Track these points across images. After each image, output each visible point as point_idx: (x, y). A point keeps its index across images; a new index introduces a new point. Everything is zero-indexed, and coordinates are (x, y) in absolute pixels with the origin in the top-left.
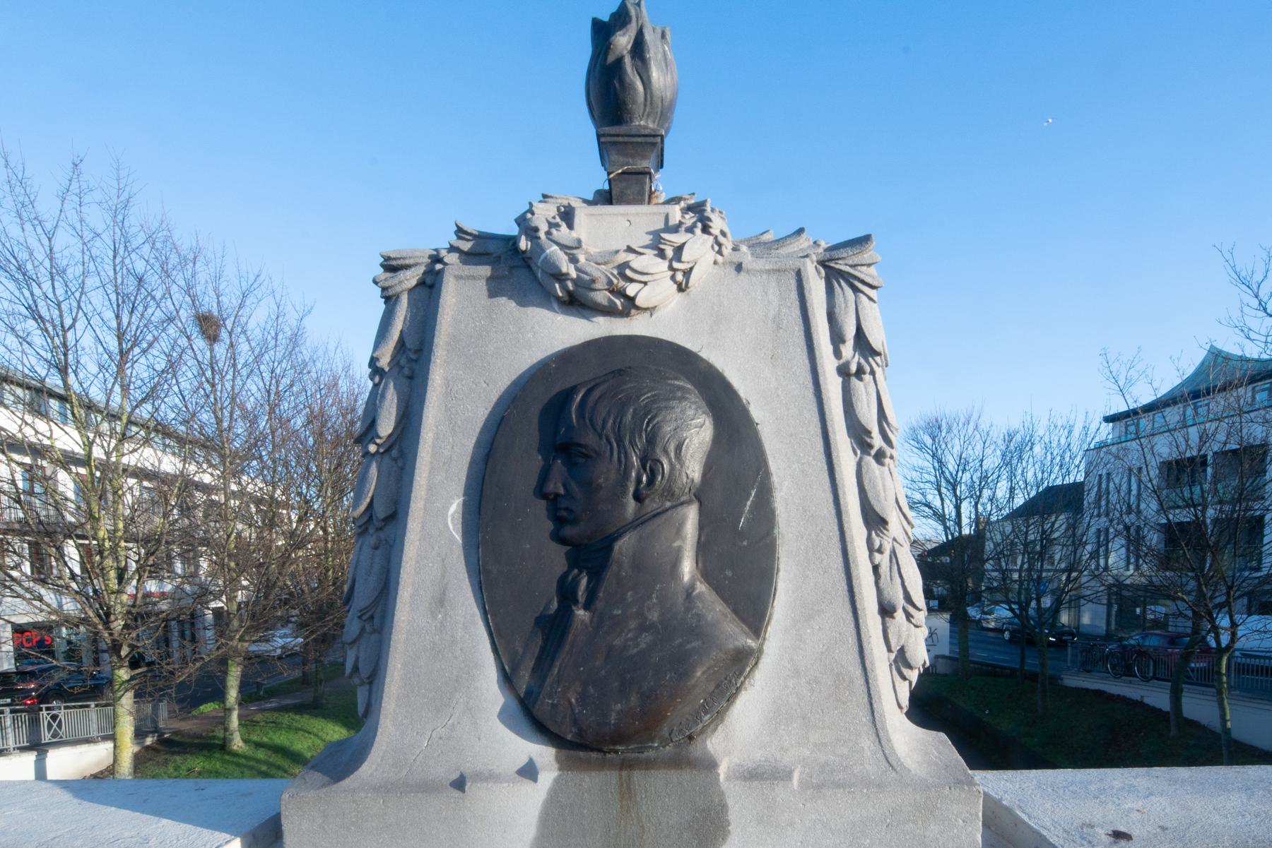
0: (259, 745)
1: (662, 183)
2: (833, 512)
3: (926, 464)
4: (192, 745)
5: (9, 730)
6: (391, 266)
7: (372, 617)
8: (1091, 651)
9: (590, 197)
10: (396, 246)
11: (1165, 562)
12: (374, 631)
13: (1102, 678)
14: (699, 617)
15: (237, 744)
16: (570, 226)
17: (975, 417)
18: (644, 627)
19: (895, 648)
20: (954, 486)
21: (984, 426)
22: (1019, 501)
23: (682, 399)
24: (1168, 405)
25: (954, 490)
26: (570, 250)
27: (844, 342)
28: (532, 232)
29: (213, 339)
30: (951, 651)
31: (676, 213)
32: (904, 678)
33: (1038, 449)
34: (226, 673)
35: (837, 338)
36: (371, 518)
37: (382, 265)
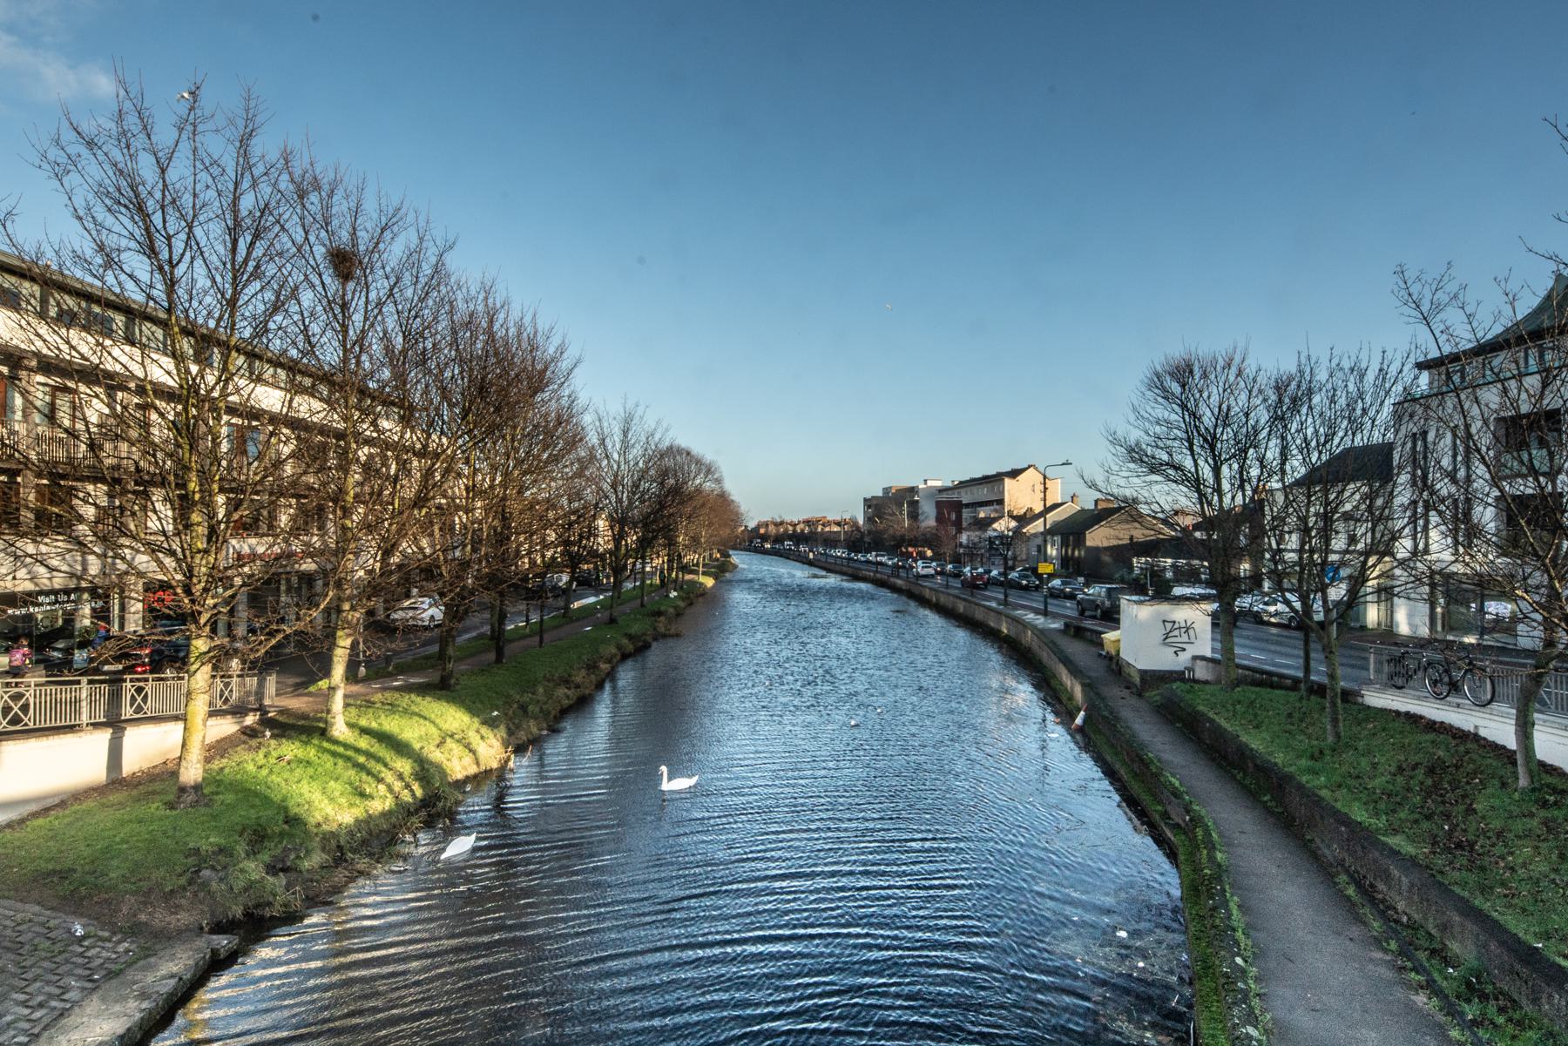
0: (365, 731)
3: (1174, 417)
4: (293, 727)
5: (84, 704)
8: (1402, 660)
11: (1511, 543)
13: (1419, 698)
15: (340, 730)
17: (1237, 359)
20: (1211, 443)
21: (1250, 371)
24: (1501, 348)
25: (1212, 448)
29: (345, 277)
30: (1213, 650)
34: (333, 645)
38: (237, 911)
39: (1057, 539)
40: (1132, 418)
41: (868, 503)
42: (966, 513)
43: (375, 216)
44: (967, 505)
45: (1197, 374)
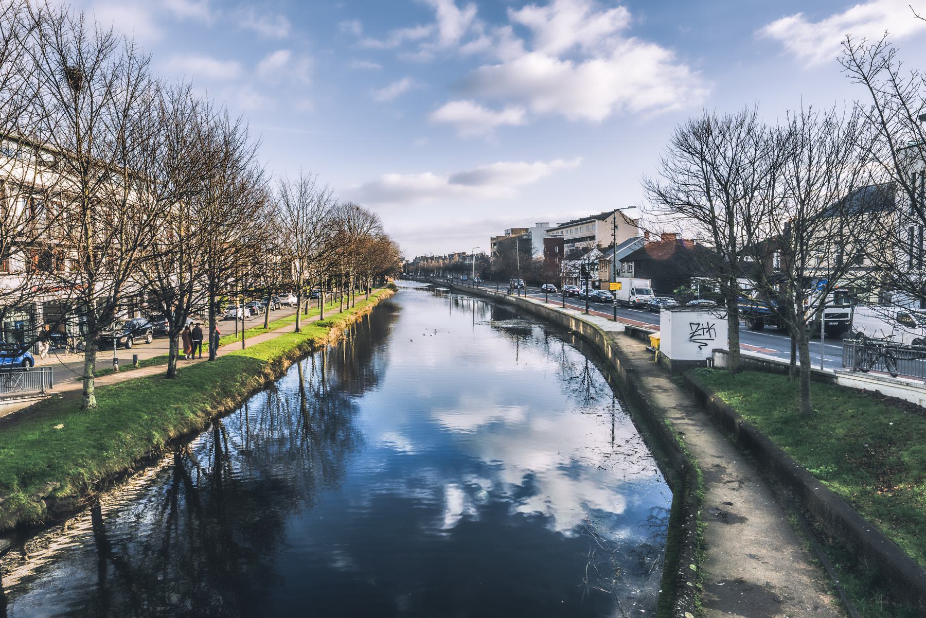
21: (758, 130)
38: (12, 523)
39: (632, 264)
40: (662, 169)
41: (496, 242)
42: (566, 248)
43: (94, 41)
44: (568, 241)
45: (715, 132)
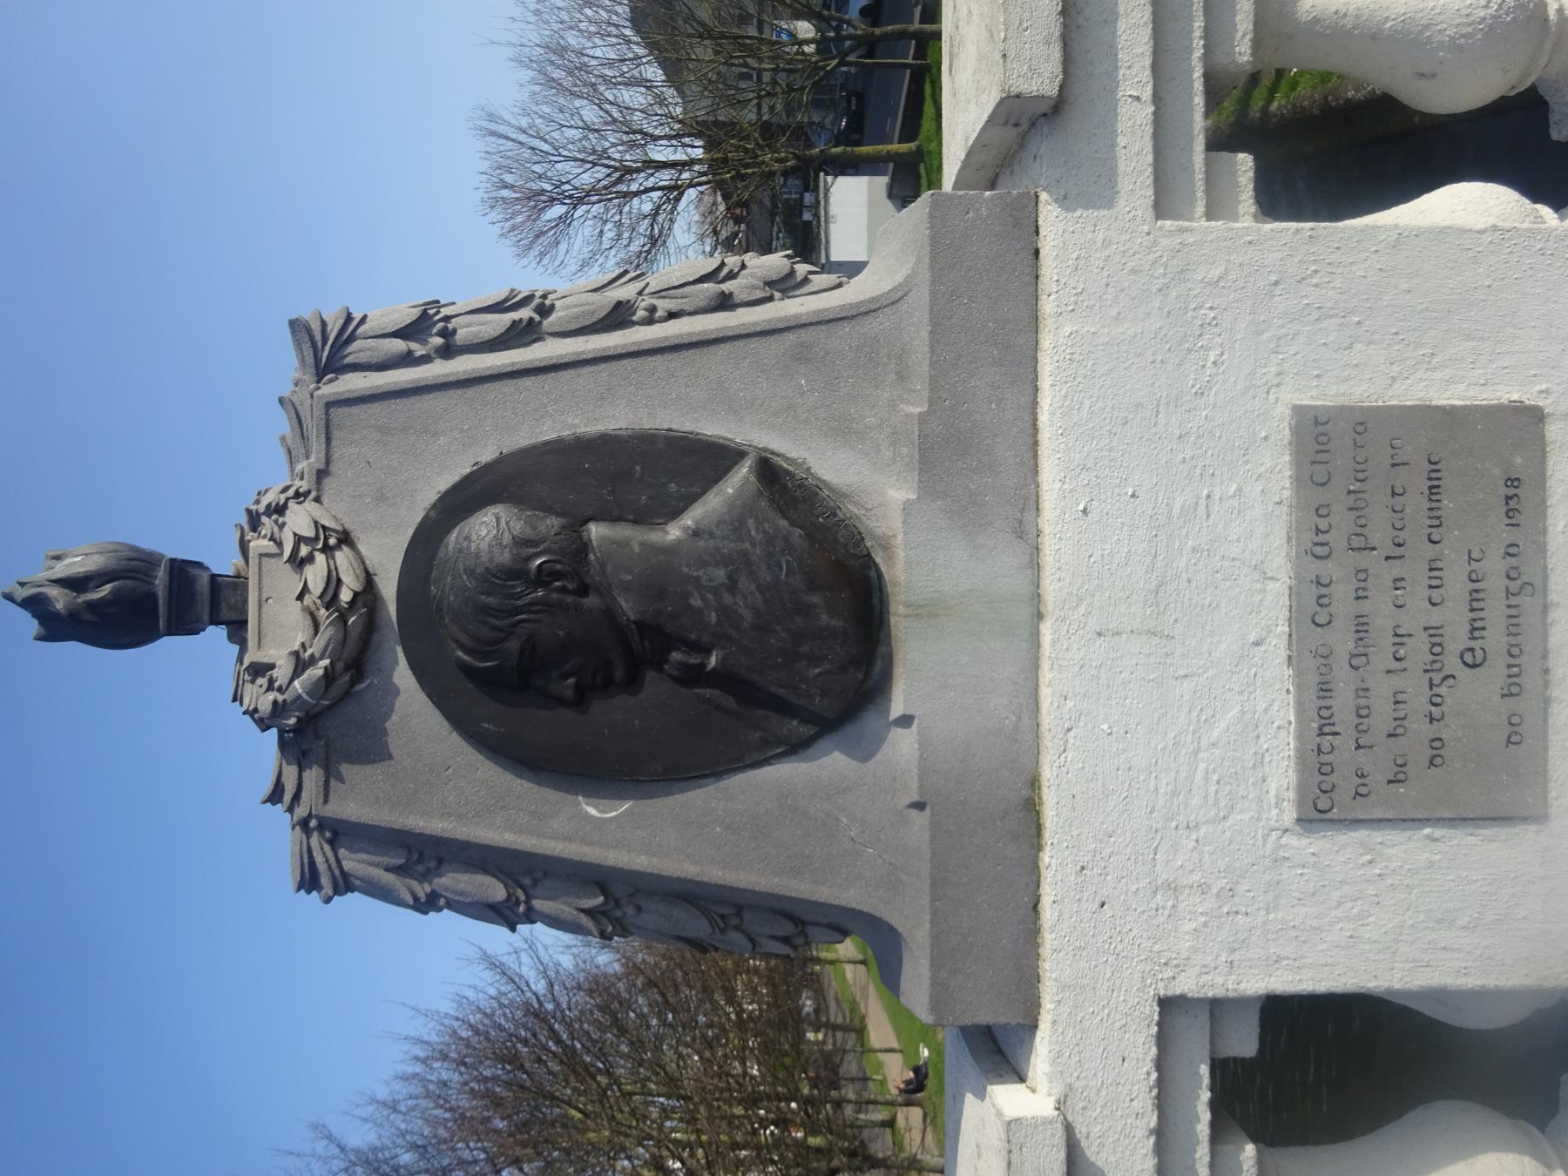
1: (224, 561)
2: (603, 366)
6: (309, 881)
7: (722, 917)
9: (236, 648)
10: (286, 871)
12: (739, 914)
14: (720, 522)
16: (272, 667)
18: (732, 587)
19: (767, 292)
20: (627, 172)
22: (654, 73)
23: (467, 538)
26: (301, 664)
27: (410, 352)
28: (278, 709)
31: (259, 544)
32: (806, 281)
33: (572, 39)
35: (407, 360)
36: (603, 913)
37: (309, 892)
